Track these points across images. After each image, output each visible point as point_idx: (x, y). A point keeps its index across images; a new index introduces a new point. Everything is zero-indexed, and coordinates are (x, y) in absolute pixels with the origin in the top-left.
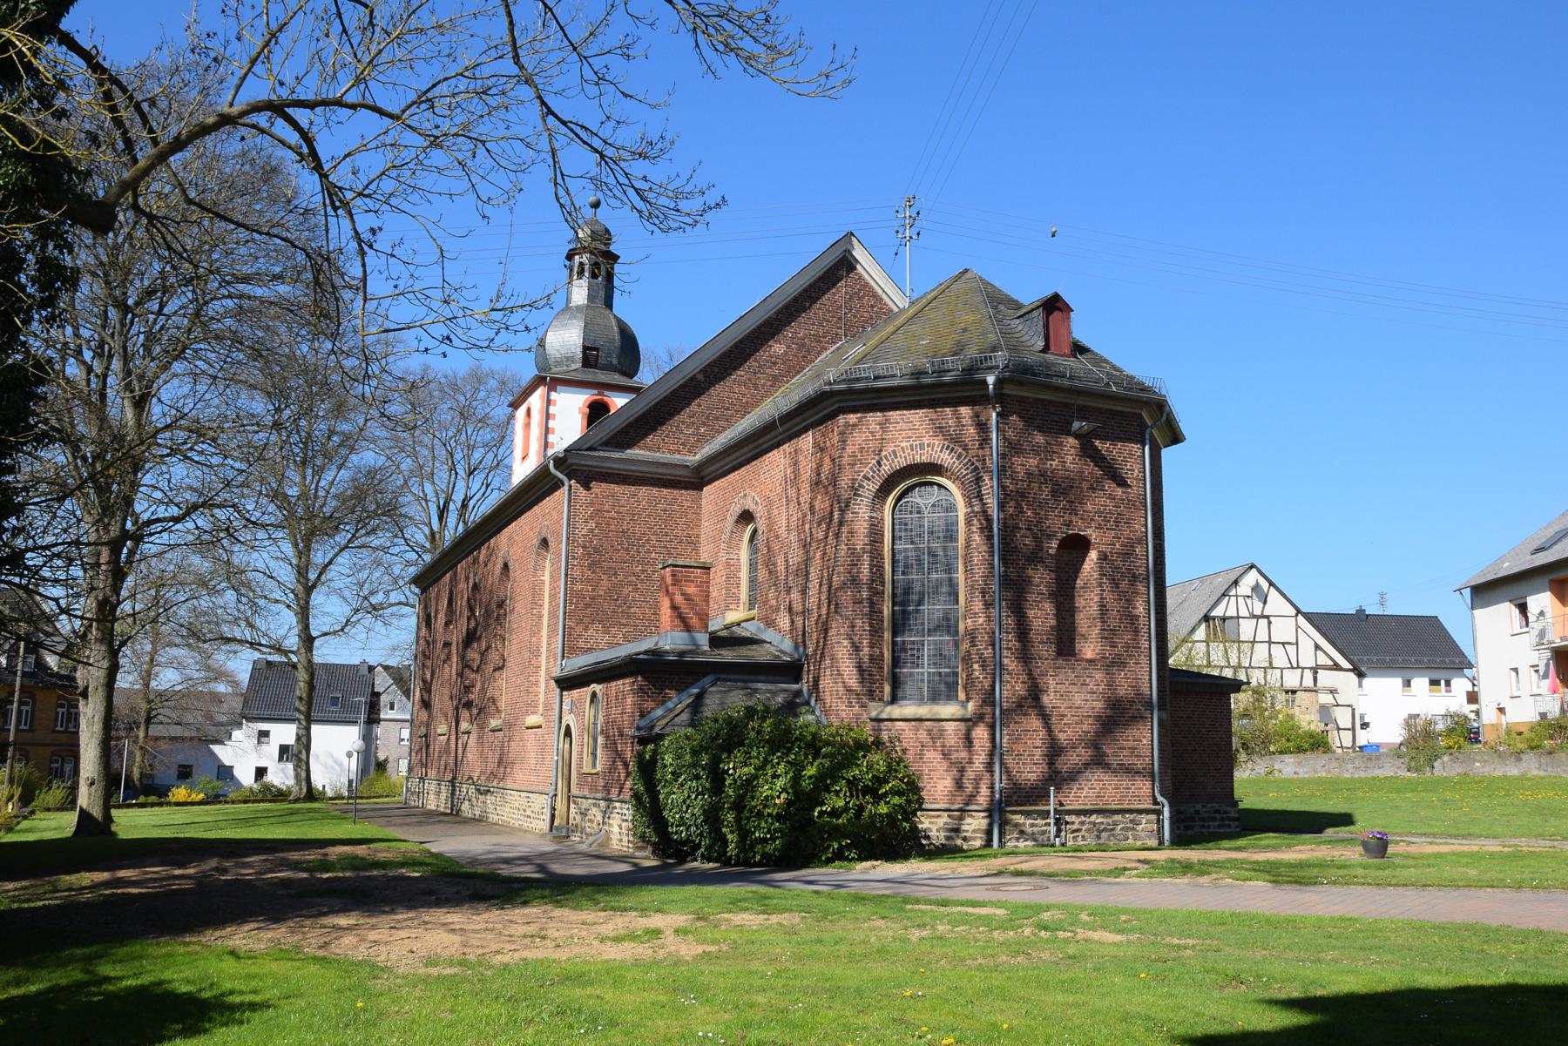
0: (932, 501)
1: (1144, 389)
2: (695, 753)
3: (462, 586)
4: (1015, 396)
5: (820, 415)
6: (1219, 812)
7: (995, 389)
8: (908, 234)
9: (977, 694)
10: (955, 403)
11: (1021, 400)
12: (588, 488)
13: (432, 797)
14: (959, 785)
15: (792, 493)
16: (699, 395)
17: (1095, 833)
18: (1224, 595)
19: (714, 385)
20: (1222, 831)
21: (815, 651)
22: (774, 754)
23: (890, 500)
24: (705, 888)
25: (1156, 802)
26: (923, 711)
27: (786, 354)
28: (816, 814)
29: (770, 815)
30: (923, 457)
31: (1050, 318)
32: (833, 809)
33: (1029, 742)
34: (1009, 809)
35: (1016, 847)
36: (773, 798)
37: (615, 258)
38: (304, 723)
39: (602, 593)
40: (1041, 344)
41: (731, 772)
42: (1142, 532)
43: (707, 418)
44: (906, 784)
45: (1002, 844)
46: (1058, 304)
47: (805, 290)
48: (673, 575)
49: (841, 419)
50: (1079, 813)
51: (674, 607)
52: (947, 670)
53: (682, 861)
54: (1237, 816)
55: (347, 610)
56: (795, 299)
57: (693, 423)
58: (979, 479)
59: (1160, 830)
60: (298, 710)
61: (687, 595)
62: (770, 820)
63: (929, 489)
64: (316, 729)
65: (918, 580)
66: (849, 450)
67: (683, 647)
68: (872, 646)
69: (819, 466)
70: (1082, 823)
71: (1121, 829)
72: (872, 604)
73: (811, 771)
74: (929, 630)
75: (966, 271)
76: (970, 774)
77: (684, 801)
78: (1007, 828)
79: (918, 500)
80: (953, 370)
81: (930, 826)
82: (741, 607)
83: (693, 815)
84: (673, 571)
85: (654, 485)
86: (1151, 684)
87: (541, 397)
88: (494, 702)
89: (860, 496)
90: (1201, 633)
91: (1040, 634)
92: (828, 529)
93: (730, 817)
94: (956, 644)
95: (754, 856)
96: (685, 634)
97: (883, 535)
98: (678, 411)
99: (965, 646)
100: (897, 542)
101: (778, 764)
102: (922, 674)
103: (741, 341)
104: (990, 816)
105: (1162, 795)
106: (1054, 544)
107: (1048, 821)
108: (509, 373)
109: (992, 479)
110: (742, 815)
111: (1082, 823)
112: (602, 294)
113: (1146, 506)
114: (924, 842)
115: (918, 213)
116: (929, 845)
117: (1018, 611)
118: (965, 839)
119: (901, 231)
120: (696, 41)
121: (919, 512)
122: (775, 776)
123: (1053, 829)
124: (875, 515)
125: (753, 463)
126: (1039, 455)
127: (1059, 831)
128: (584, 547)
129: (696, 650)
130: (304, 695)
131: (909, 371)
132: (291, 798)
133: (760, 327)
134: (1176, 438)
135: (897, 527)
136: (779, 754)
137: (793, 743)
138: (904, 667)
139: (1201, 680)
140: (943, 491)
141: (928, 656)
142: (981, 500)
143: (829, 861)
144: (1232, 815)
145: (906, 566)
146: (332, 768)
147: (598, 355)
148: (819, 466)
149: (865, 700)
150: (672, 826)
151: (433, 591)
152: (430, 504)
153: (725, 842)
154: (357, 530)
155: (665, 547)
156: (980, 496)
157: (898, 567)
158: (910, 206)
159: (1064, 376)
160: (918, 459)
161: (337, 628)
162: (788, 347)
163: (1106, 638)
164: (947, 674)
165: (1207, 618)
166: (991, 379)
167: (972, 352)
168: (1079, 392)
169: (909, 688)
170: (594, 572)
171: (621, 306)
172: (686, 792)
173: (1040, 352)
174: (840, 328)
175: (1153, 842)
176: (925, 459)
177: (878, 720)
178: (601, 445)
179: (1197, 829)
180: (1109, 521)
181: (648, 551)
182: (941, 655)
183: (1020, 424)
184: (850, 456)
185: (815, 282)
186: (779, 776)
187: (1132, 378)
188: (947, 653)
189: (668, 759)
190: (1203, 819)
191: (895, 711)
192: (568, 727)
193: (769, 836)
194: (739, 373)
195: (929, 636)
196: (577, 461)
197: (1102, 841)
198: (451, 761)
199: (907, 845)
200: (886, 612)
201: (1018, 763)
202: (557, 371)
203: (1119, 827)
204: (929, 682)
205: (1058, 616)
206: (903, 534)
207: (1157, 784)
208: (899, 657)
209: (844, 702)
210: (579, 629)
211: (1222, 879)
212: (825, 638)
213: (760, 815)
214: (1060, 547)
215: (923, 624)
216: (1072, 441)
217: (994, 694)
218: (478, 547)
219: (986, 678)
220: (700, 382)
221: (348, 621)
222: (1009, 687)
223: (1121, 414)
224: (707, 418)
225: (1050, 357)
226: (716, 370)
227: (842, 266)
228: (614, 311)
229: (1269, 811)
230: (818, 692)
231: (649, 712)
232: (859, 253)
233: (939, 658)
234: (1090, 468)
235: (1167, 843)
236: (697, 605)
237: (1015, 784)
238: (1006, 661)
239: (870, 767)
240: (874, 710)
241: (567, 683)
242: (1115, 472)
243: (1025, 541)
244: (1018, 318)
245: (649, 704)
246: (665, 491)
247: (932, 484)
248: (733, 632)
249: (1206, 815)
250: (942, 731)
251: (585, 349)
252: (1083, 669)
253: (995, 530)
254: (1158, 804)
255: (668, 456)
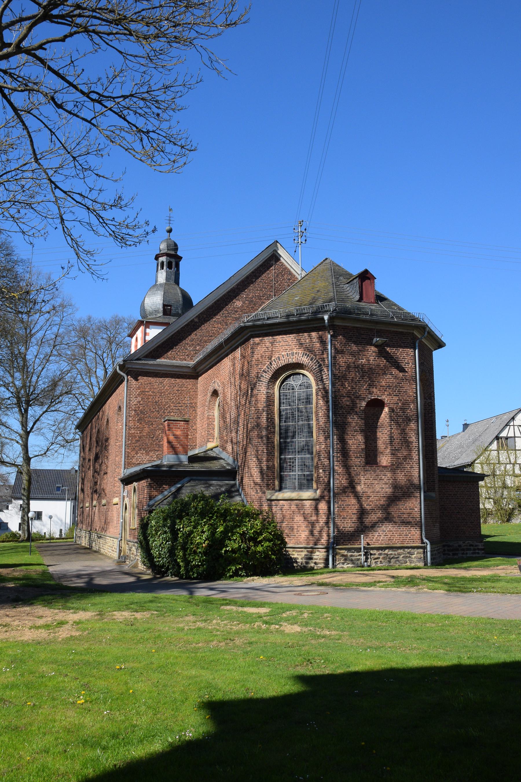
0: (300, 383)
1: (414, 319)
2: (165, 520)
3: (94, 431)
4: (341, 326)
5: (243, 339)
6: (472, 546)
7: (328, 322)
8: (300, 241)
9: (322, 486)
10: (309, 330)
11: (345, 328)
12: (137, 380)
13: (84, 539)
14: (312, 533)
15: (232, 380)
16: (196, 330)
17: (388, 560)
18: (507, 425)
19: (204, 324)
20: (474, 556)
21: (241, 463)
22: (202, 520)
23: (278, 383)
24: (138, 594)
25: (423, 542)
26: (294, 495)
27: (242, 306)
28: (223, 552)
29: (200, 552)
30: (293, 360)
31: (364, 283)
32: (232, 549)
33: (350, 511)
34: (337, 547)
35: (342, 567)
36: (201, 544)
37: (181, 258)
38: (26, 501)
39: (145, 434)
40: (358, 297)
41: (181, 530)
42: (414, 396)
43: (200, 341)
44: (273, 535)
45: (334, 566)
46: (367, 276)
47: (253, 272)
48: (168, 425)
49: (252, 341)
50: (378, 549)
51: (169, 442)
52: (308, 473)
53: (163, 576)
54: (483, 547)
55: (47, 443)
56: (247, 277)
57: (193, 344)
58: (321, 371)
59: (425, 558)
60: (23, 495)
61: (176, 435)
62: (200, 555)
63: (298, 376)
64: (32, 502)
65: (292, 425)
66: (256, 357)
67: (173, 463)
68: (268, 461)
69: (243, 366)
70: (380, 554)
71: (403, 557)
72: (268, 438)
73: (221, 529)
74: (298, 452)
75: (326, 259)
76: (317, 528)
77: (160, 545)
78: (337, 557)
79: (292, 383)
80: (308, 313)
81: (298, 556)
82: (215, 440)
83: (165, 552)
84: (168, 423)
85: (172, 377)
86: (420, 478)
87: (142, 332)
88: (104, 490)
89: (262, 381)
90: (494, 446)
91: (356, 453)
92: (246, 399)
93: (181, 554)
94: (312, 459)
95: (193, 574)
96: (175, 456)
97: (274, 402)
98: (184, 338)
99: (316, 460)
100: (282, 405)
101: (204, 525)
102: (295, 475)
103: (218, 300)
104: (328, 551)
105: (426, 539)
106: (364, 404)
107: (360, 553)
108: (132, 319)
109: (328, 371)
110: (187, 553)
111: (380, 554)
112: (173, 277)
113: (416, 382)
114: (295, 565)
115: (305, 230)
116: (297, 567)
117: (342, 441)
118: (315, 563)
119: (296, 239)
120: (143, 145)
121: (293, 389)
122: (203, 532)
123: (363, 558)
124: (269, 391)
125: (218, 365)
126: (355, 357)
127: (367, 559)
128: (135, 411)
129: (180, 464)
130: (26, 487)
131: (285, 314)
132: (20, 540)
133: (229, 292)
134: (440, 345)
135: (282, 397)
136: (205, 520)
137: (213, 514)
138: (285, 472)
139: (464, 475)
140: (305, 378)
141: (298, 465)
142: (323, 382)
143: (231, 577)
144: (480, 547)
145: (286, 418)
146: (57, 522)
147: (171, 309)
148: (243, 366)
149: (265, 489)
150: (156, 558)
151: (85, 433)
152: (94, 387)
153: (180, 567)
154: (52, 402)
155: (178, 409)
156: (322, 380)
157: (282, 418)
158: (301, 226)
159: (368, 314)
160: (291, 361)
161: (43, 453)
162: (244, 303)
163: (394, 454)
164: (308, 475)
165: (497, 438)
166: (326, 317)
167: (319, 303)
168: (377, 323)
169: (288, 483)
170: (141, 423)
171: (183, 284)
172: (161, 540)
173: (357, 301)
174: (272, 291)
175: (421, 564)
176: (294, 361)
177: (271, 500)
178: (144, 357)
179: (460, 555)
180: (395, 391)
181: (170, 412)
182: (305, 465)
183: (344, 341)
184: (256, 360)
185: (258, 268)
186: (205, 532)
187: (409, 313)
188: (308, 464)
189: (153, 522)
190: (463, 550)
191: (280, 495)
192: (126, 504)
193: (200, 564)
194: (217, 317)
195: (298, 455)
196: (131, 366)
197: (392, 564)
198: (90, 521)
199: (277, 567)
200: (276, 442)
201: (343, 523)
202: (150, 318)
203: (402, 556)
204: (298, 479)
205: (366, 443)
206: (285, 401)
207: (423, 532)
208: (283, 466)
209: (254, 491)
210: (133, 453)
211: (422, 589)
212: (245, 457)
213: (195, 552)
214: (367, 405)
215: (295, 448)
216: (373, 348)
217: (330, 485)
218: (99, 411)
219: (326, 477)
220: (196, 322)
221: (48, 449)
222: (338, 482)
223: (401, 333)
224: (200, 341)
225: (362, 304)
226: (205, 316)
227: (274, 258)
228: (181, 285)
229: (515, 543)
230: (243, 486)
231: (154, 497)
232: (281, 252)
233: (304, 466)
234: (383, 362)
235: (429, 565)
236: (181, 440)
237: (342, 534)
238: (336, 468)
239: (252, 527)
240: (269, 494)
241: (127, 481)
242: (398, 365)
243: (346, 401)
244: (348, 283)
245: (155, 493)
246: (178, 380)
247: (299, 374)
248: (207, 454)
249: (465, 547)
250: (303, 505)
251: (164, 306)
252: (380, 471)
253: (330, 398)
254: (424, 543)
255: (180, 362)
